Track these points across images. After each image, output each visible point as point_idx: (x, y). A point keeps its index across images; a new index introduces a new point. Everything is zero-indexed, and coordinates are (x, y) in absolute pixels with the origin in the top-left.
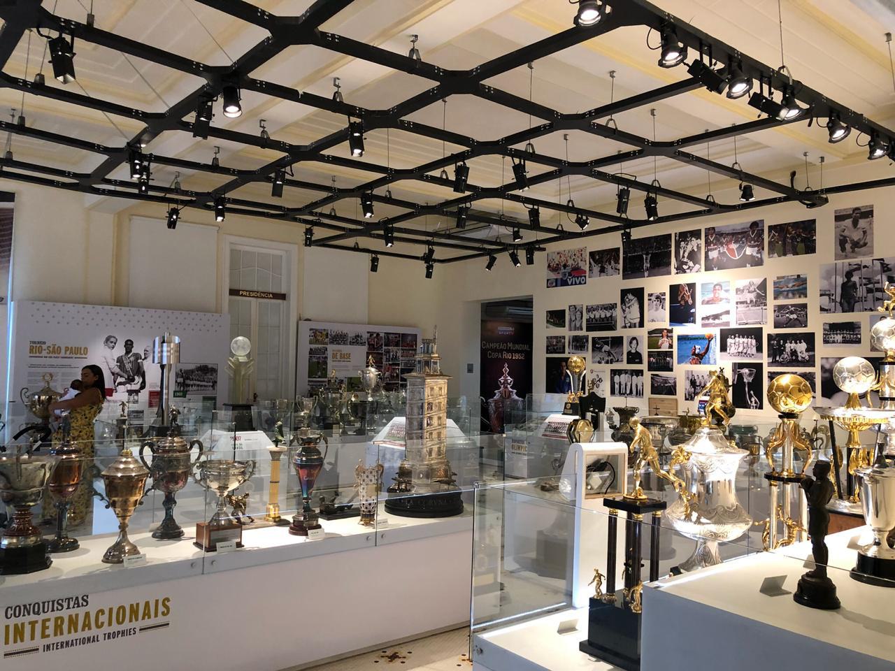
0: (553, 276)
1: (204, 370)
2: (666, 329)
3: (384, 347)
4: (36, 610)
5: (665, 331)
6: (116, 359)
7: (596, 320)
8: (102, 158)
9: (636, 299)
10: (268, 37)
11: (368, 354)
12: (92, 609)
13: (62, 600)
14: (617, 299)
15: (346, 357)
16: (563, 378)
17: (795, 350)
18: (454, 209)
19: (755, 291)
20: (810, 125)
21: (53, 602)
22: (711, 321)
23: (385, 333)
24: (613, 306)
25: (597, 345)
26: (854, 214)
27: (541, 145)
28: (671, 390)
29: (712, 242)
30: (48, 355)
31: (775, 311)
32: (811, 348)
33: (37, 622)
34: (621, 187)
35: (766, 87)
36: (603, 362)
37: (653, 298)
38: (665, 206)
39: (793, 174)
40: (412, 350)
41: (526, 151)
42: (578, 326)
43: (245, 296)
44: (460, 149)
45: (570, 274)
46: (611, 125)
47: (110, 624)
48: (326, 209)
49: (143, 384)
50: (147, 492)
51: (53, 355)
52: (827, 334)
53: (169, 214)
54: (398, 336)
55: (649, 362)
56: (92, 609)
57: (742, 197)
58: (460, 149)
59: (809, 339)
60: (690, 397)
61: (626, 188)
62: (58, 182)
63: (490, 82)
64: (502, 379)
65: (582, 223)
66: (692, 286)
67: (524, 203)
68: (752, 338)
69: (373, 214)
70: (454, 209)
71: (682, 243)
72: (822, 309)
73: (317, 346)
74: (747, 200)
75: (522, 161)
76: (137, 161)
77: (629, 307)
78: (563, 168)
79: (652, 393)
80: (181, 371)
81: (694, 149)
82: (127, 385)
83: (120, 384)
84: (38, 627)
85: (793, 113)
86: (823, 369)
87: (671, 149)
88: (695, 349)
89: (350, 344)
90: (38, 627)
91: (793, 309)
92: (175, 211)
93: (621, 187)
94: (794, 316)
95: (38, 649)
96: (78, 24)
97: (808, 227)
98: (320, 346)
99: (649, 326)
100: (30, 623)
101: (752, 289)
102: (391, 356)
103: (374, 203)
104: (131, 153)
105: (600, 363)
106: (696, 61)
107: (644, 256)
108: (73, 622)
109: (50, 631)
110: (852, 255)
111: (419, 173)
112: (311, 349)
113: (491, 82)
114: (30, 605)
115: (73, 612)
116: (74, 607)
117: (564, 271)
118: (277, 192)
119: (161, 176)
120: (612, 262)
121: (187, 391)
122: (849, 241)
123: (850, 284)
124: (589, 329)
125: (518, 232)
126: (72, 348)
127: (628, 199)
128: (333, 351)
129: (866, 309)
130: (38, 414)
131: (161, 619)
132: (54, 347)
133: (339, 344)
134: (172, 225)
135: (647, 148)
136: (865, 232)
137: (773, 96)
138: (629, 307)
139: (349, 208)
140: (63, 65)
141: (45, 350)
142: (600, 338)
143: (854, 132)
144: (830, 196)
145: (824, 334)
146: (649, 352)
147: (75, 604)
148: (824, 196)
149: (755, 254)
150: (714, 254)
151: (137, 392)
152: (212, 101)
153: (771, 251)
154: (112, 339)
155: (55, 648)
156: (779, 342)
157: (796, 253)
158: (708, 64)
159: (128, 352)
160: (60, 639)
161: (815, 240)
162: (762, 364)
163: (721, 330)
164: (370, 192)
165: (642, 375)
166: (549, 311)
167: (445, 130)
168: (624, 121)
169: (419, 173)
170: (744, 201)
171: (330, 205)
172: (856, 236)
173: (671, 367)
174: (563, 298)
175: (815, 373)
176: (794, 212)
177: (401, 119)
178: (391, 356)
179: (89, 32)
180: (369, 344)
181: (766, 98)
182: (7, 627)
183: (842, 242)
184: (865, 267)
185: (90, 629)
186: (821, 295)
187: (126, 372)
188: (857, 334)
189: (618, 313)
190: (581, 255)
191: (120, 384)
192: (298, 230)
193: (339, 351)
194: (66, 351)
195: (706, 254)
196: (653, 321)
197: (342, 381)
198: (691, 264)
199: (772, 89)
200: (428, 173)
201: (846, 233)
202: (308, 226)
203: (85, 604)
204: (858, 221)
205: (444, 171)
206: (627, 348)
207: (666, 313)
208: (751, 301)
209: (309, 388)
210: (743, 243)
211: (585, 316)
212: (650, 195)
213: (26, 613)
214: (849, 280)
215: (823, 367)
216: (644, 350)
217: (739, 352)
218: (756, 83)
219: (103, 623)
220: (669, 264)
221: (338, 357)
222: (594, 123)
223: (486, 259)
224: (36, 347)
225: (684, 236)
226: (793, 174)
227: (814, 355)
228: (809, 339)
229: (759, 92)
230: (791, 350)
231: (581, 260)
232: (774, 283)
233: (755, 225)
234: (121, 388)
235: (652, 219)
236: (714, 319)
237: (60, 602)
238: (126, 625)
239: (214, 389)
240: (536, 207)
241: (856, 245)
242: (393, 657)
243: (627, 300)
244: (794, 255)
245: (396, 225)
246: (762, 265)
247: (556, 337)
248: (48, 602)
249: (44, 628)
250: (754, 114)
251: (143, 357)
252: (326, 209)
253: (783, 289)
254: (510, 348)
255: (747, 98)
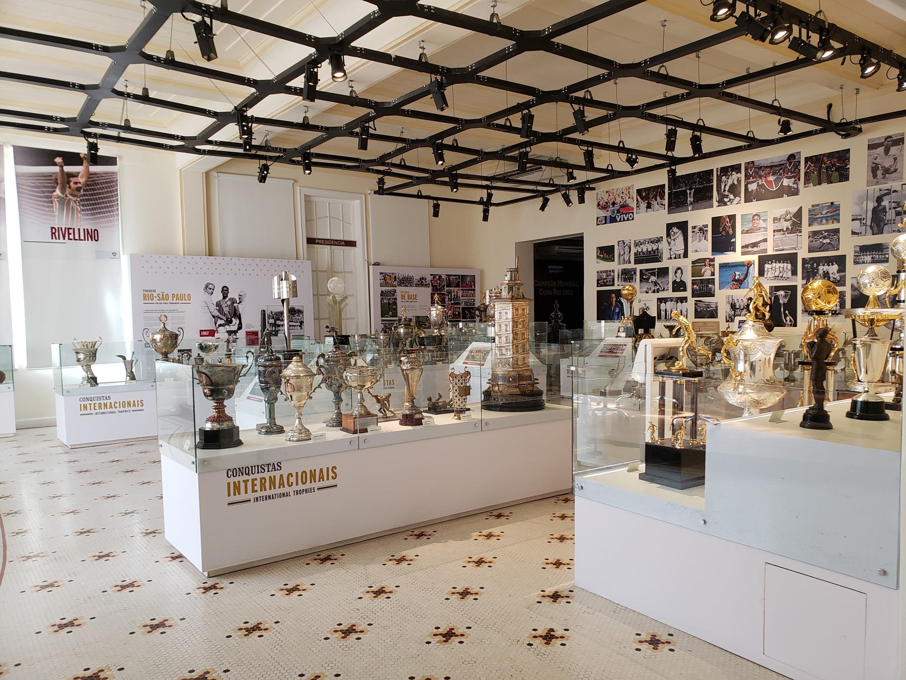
0: (602, 214)
1: (292, 311)
2: (708, 258)
3: (446, 288)
4: (247, 472)
5: (708, 260)
6: (215, 304)
7: (644, 254)
8: (210, 121)
9: (680, 231)
10: (374, 11)
11: (433, 295)
12: (284, 472)
13: (264, 465)
14: (664, 234)
15: (413, 298)
16: (612, 308)
17: (828, 272)
18: (515, 153)
19: (791, 219)
20: (843, 64)
21: (258, 466)
22: (750, 249)
23: (446, 275)
24: (659, 240)
25: (644, 276)
26: (886, 142)
27: (599, 93)
28: (713, 314)
29: (751, 176)
30: (159, 302)
31: (809, 237)
32: (842, 269)
33: (248, 480)
34: (670, 127)
35: (804, 31)
36: (650, 292)
37: (696, 230)
38: (709, 143)
39: (830, 106)
40: (471, 290)
41: (584, 98)
42: (626, 259)
43: (320, 244)
44: (524, 98)
45: (618, 212)
46: (663, 71)
47: (297, 484)
48: (396, 160)
49: (240, 326)
50: (315, 389)
51: (163, 302)
52: (858, 256)
53: (261, 170)
54: (458, 277)
55: (693, 289)
56: (284, 472)
57: (781, 131)
58: (524, 98)
59: (841, 261)
60: (730, 319)
61: (674, 128)
62: (166, 145)
63: (558, 40)
64: (553, 315)
65: (632, 162)
66: (732, 218)
67: (579, 145)
68: (787, 263)
69: (444, 161)
70: (515, 153)
71: (724, 177)
72: (853, 233)
73: (387, 288)
74: (785, 134)
75: (582, 107)
76: (244, 123)
77: (674, 240)
78: (618, 111)
79: (695, 318)
80: (272, 313)
81: (738, 90)
82: (227, 326)
83: (220, 325)
84: (249, 484)
85: (828, 54)
86: (853, 288)
87: (717, 91)
88: (735, 276)
89: (416, 286)
90: (249, 484)
91: (826, 234)
92: (266, 168)
93: (670, 127)
94: (828, 241)
95: (250, 500)
96: (215, 8)
97: (843, 156)
98: (390, 288)
99: (692, 256)
100: (244, 481)
101: (788, 217)
102: (453, 297)
103: (445, 152)
104: (240, 116)
105: (647, 292)
106: (743, 12)
107: (688, 191)
108: (272, 481)
109: (257, 488)
110: (883, 181)
111: (488, 122)
112: (382, 292)
113: (561, 39)
114: (243, 468)
115: (272, 474)
116: (272, 471)
117: (612, 209)
118: (363, 146)
119: (260, 134)
120: (658, 198)
121: (278, 330)
122: (880, 168)
123: (880, 208)
124: (636, 262)
125: (572, 172)
126: (177, 295)
127: (675, 138)
128: (401, 292)
129: (894, 231)
130: (290, 307)
131: (331, 482)
132: (163, 295)
133: (407, 286)
134: (263, 179)
135: (695, 90)
136: (895, 159)
137: (810, 39)
138: (674, 240)
139: (423, 158)
140: (207, 46)
141: (155, 297)
142: (647, 270)
143: (884, 67)
144: (864, 126)
145: (854, 256)
146: (692, 280)
147: (273, 468)
148: (858, 126)
149: (791, 185)
150: (753, 187)
151: (235, 332)
152: (318, 67)
153: (807, 181)
154: (210, 286)
155: (261, 500)
156: (812, 264)
157: (830, 182)
158: (753, 15)
159: (224, 297)
160: (264, 493)
161: (849, 168)
162: (796, 286)
163: (759, 256)
164: (440, 141)
165: (686, 302)
166: (599, 247)
167: (507, 80)
168: (673, 68)
169: (488, 122)
170: (782, 135)
171: (400, 157)
172: (887, 163)
173: (712, 293)
174: (611, 235)
175: (845, 292)
176: (830, 143)
177: (478, 74)
178: (453, 297)
179: (224, 14)
180: (432, 285)
181: (803, 41)
182: (229, 484)
183: (874, 170)
184: (895, 191)
185: (284, 487)
186: (853, 220)
187: (225, 315)
188: (885, 254)
189: (664, 246)
190: (629, 193)
191: (220, 325)
192: (372, 180)
193: (407, 292)
194: (173, 298)
195: (746, 186)
196: (696, 251)
197: (411, 319)
198: (732, 197)
199: (810, 32)
200: (494, 122)
201: (877, 161)
202: (380, 176)
203: (279, 468)
204: (890, 148)
205: (508, 119)
206: (673, 278)
207: (709, 244)
208: (787, 229)
209: (383, 326)
210: (781, 175)
211: (634, 250)
212: (696, 133)
213: (240, 474)
214: (879, 204)
215: (852, 286)
216: (688, 279)
217: (775, 276)
218: (795, 28)
219: (292, 483)
220: (711, 197)
221: (406, 298)
222: (648, 71)
223: (539, 201)
224: (148, 295)
225: (725, 171)
226: (830, 106)
227: (845, 276)
228: (841, 261)
229: (798, 36)
230: (824, 272)
231: (629, 198)
232: (809, 211)
233: (792, 157)
234: (221, 329)
235: (697, 155)
236: (753, 247)
237: (263, 466)
238: (308, 485)
239: (301, 329)
240: (590, 149)
241: (887, 171)
242: (499, 516)
243: (672, 233)
244: (828, 183)
245: (459, 172)
246: (798, 194)
247: (606, 272)
248: (255, 466)
249: (254, 485)
250: (793, 56)
251: (238, 302)
252: (396, 160)
253: (818, 216)
254: (560, 285)
255: (787, 43)
